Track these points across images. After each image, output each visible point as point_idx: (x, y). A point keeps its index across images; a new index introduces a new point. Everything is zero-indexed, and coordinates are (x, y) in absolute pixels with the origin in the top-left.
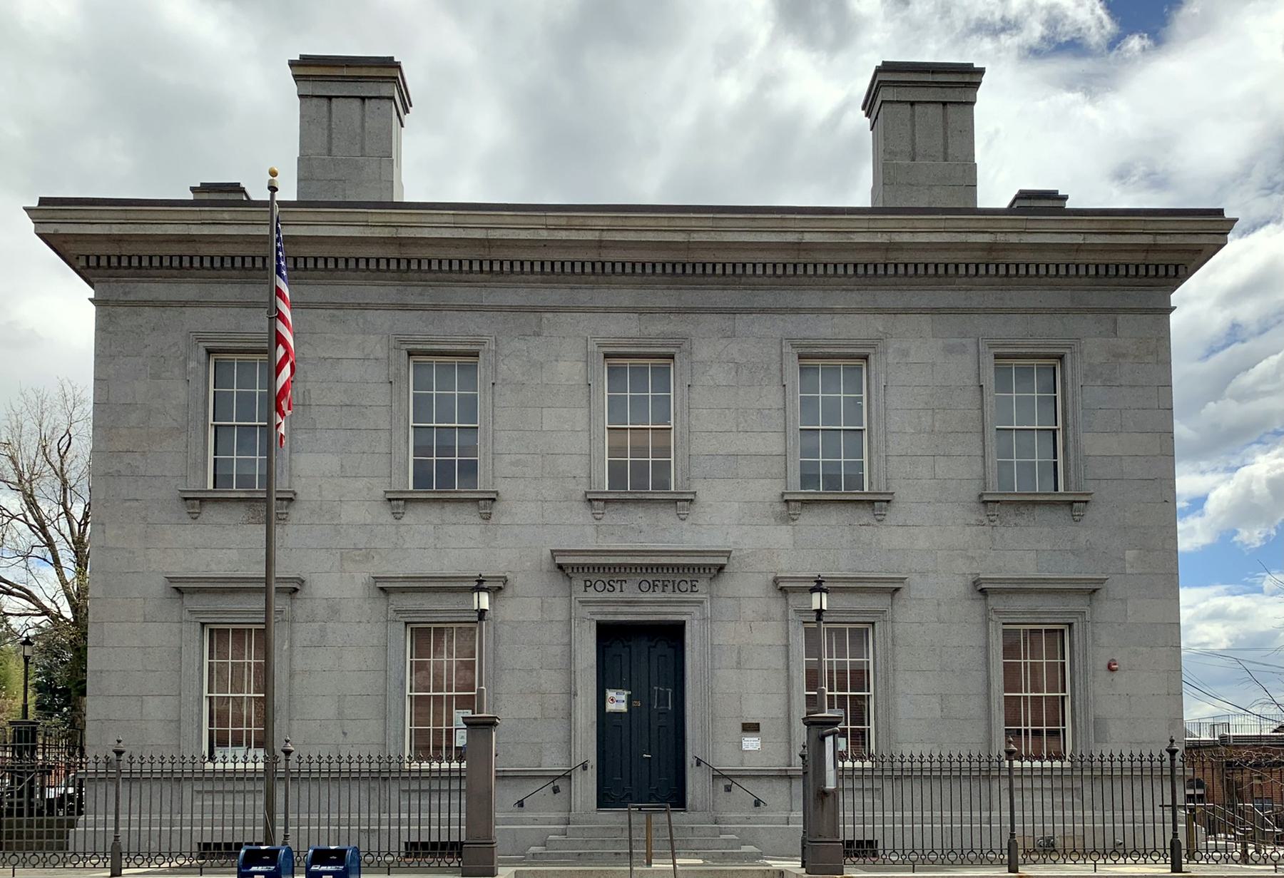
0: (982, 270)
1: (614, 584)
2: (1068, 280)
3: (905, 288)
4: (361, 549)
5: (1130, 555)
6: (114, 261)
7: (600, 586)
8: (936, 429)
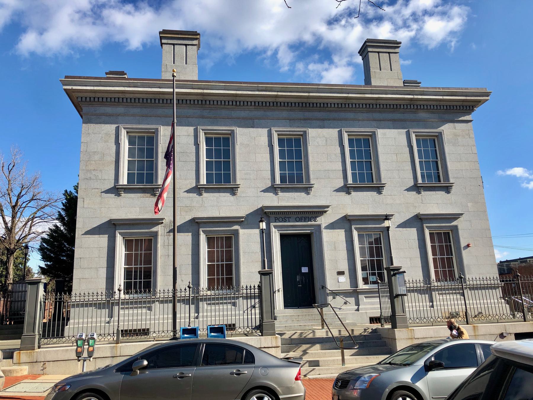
0: (409, 107)
1: (286, 219)
2: (383, 110)
3: (382, 112)
4: (188, 207)
5: (470, 205)
6: (92, 99)
7: (280, 219)
8: (398, 160)
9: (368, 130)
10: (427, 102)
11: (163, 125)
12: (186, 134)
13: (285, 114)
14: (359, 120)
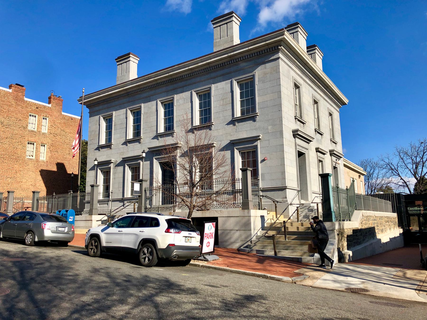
5: (270, 127)
9: (207, 87)
12: (123, 113)
13: (164, 89)
14: (202, 81)
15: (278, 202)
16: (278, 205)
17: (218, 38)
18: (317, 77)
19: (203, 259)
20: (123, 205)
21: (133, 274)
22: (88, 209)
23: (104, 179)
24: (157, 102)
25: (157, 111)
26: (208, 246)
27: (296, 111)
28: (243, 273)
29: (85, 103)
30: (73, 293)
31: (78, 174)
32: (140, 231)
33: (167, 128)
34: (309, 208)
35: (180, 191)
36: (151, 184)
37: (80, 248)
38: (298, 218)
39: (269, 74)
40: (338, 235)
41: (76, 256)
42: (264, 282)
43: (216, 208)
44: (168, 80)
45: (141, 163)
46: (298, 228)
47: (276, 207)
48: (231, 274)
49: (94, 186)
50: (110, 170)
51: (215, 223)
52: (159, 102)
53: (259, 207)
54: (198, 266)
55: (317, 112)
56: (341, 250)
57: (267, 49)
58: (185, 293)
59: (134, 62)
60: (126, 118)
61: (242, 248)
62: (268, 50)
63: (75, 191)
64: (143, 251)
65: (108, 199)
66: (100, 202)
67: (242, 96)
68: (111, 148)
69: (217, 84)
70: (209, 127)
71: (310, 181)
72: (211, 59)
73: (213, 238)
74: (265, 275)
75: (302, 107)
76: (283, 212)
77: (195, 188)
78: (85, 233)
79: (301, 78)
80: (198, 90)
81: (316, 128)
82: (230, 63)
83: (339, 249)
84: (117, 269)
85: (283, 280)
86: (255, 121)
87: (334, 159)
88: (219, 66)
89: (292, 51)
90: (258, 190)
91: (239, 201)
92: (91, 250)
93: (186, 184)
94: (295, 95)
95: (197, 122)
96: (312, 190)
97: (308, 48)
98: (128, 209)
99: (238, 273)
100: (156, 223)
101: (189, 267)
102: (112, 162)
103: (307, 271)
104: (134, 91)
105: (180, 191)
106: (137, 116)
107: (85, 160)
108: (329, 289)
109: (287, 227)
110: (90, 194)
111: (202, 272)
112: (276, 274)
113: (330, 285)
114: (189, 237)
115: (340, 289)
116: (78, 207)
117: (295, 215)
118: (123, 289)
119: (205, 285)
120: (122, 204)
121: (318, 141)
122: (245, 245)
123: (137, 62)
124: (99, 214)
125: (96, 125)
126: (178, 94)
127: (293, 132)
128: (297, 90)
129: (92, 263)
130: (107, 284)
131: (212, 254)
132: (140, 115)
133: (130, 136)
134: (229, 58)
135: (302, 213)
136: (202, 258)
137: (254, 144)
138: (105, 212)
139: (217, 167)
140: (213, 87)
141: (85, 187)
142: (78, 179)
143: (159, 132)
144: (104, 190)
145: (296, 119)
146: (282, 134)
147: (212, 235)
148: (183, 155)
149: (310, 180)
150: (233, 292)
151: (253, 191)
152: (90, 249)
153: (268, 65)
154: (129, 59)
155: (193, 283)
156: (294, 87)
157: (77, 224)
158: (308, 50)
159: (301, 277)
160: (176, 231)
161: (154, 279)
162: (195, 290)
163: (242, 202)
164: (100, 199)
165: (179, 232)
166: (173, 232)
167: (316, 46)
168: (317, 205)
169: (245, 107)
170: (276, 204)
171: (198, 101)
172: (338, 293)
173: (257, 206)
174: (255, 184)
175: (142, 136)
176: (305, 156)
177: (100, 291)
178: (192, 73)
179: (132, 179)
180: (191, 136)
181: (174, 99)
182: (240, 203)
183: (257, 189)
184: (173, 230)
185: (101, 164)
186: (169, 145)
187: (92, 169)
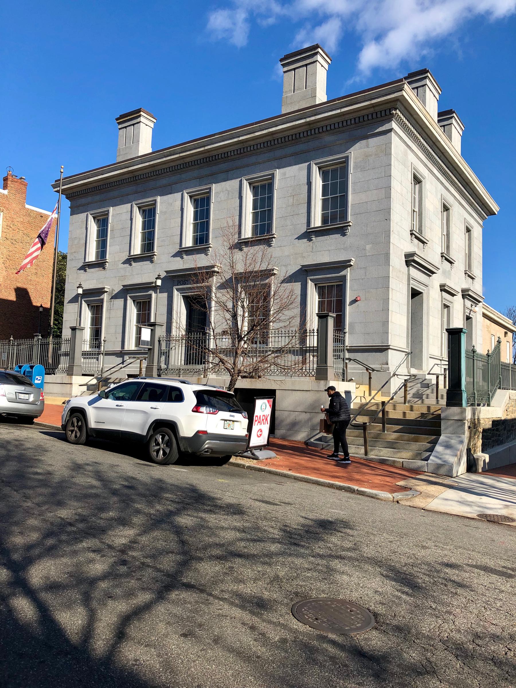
3: (284, 147)
5: (368, 247)
9: (267, 173)
10: (329, 121)
11: (112, 207)
12: (125, 211)
14: (259, 163)
15: (373, 370)
16: (373, 374)
17: (290, 90)
18: (451, 167)
19: (251, 455)
20: (123, 363)
21: (138, 476)
22: (66, 366)
23: (92, 319)
24: (182, 194)
25: (182, 210)
26: (259, 435)
27: (414, 221)
28: (314, 482)
29: (64, 191)
30: (45, 503)
31: (49, 307)
32: (151, 408)
33: (197, 239)
34: (423, 381)
35: (218, 346)
36: (169, 330)
37: (53, 427)
38: (405, 397)
39: (373, 157)
40: (469, 428)
41: (48, 442)
42: (348, 498)
43: (273, 374)
44: (203, 159)
45: (154, 295)
46: (404, 414)
47: (370, 378)
48: (295, 482)
49: (76, 329)
50: (101, 304)
51: (272, 400)
52: (186, 194)
53: (344, 377)
54: (242, 466)
55: (447, 225)
56: (472, 452)
57: (372, 114)
58: (223, 513)
59: (146, 125)
60: (131, 219)
61: (312, 440)
62: (374, 116)
63: (45, 336)
64: (156, 440)
65: (99, 351)
66: (85, 354)
67: (325, 192)
68: (104, 268)
69: (284, 169)
70: (268, 242)
71: (428, 339)
72: (276, 126)
73: (268, 424)
74: (349, 488)
75: (423, 216)
76: (382, 387)
77: (243, 342)
78: (60, 403)
79: (426, 166)
80: (252, 177)
81: (443, 252)
82: (309, 134)
83: (469, 450)
84: (112, 466)
85: (378, 497)
86: (344, 235)
87: (468, 303)
88: (290, 138)
89: (414, 119)
90: (344, 349)
91: (311, 366)
92: (72, 433)
93: (224, 333)
94: (413, 195)
95: (248, 232)
96: (430, 353)
97: (440, 115)
98: (130, 368)
99: (305, 482)
100: (177, 395)
101: (228, 468)
102: (107, 292)
103: (417, 484)
104: (145, 175)
105: (216, 346)
106: (150, 216)
107: (61, 285)
108: (451, 515)
109: (387, 412)
110: (69, 342)
111: (249, 478)
112: (367, 486)
113: (453, 508)
114: (230, 421)
115: (469, 515)
116: (50, 361)
117: (402, 392)
118: (124, 501)
119: (254, 500)
120: (120, 360)
121: (445, 273)
122: (317, 437)
123: (152, 125)
124: (83, 375)
125: (82, 228)
126: (218, 183)
127: (405, 257)
128: (417, 186)
129: (73, 454)
130: (98, 491)
131: (265, 449)
132: (154, 216)
133: (137, 250)
134: (307, 125)
135: (411, 389)
136: (248, 454)
137: (341, 273)
138: (93, 371)
139: (280, 310)
140: (278, 173)
141: (62, 329)
142: (50, 316)
143: (183, 246)
144: (91, 336)
145: (411, 234)
146: (387, 260)
147: (266, 419)
148: (222, 286)
149: (428, 336)
150: (301, 514)
151: (335, 350)
152: (70, 431)
153: (372, 141)
154: (138, 120)
155: (236, 496)
156: (413, 181)
157: (47, 388)
158: (439, 119)
159: (408, 493)
160: (210, 410)
161: (173, 485)
162: (240, 507)
163: (316, 368)
164: (85, 350)
165: (214, 412)
166: (205, 412)
167: (454, 112)
168: (437, 377)
169: (330, 211)
170: (370, 373)
171: (252, 196)
172: (466, 521)
173: (340, 375)
174: (339, 340)
175: (155, 250)
176: (422, 297)
177: (87, 503)
178: (244, 148)
179: (138, 321)
180: (238, 255)
181: (212, 191)
182: (313, 370)
183: (342, 347)
184: (205, 408)
185: (88, 293)
186: (200, 268)
187: (75, 300)
